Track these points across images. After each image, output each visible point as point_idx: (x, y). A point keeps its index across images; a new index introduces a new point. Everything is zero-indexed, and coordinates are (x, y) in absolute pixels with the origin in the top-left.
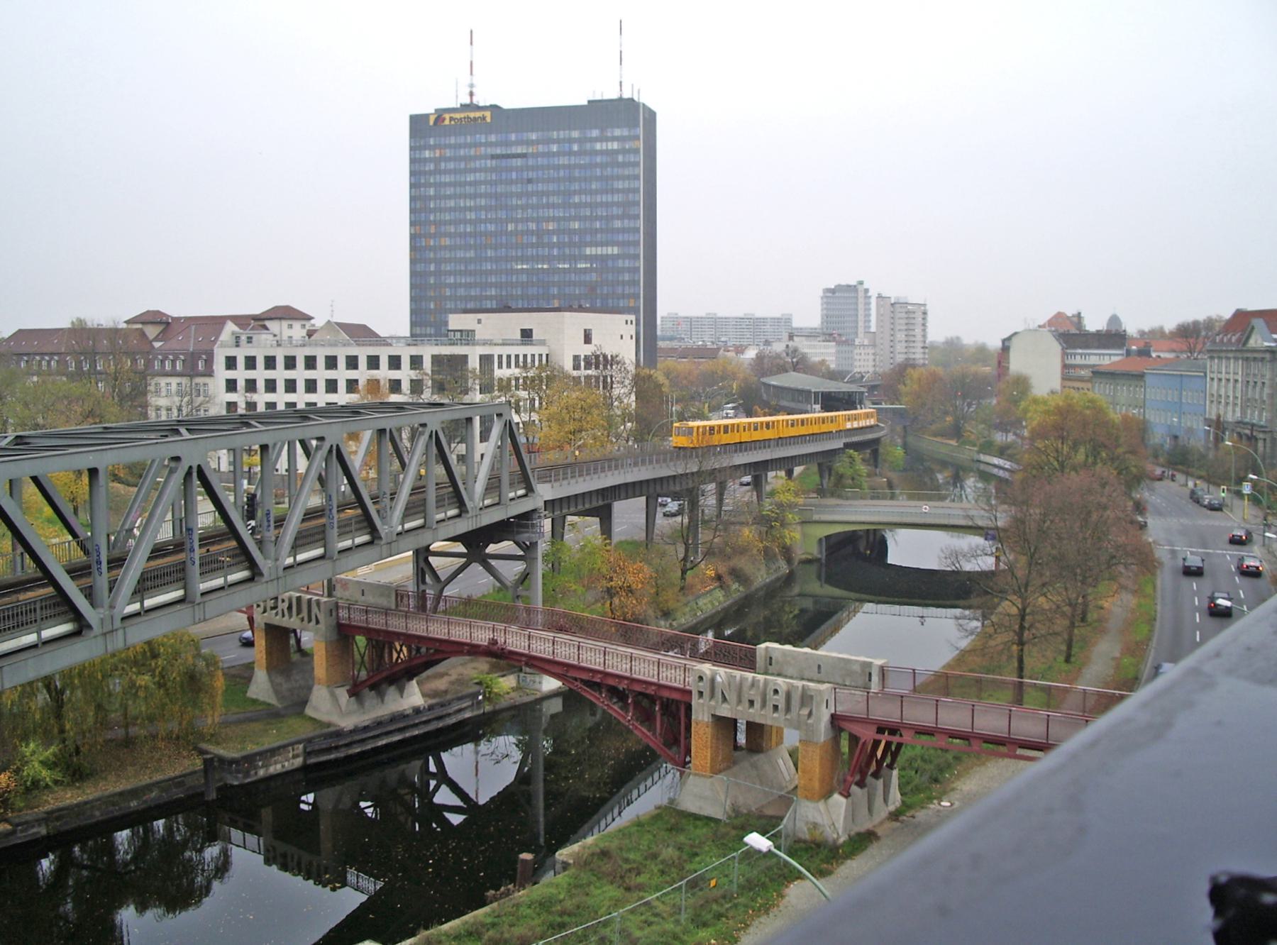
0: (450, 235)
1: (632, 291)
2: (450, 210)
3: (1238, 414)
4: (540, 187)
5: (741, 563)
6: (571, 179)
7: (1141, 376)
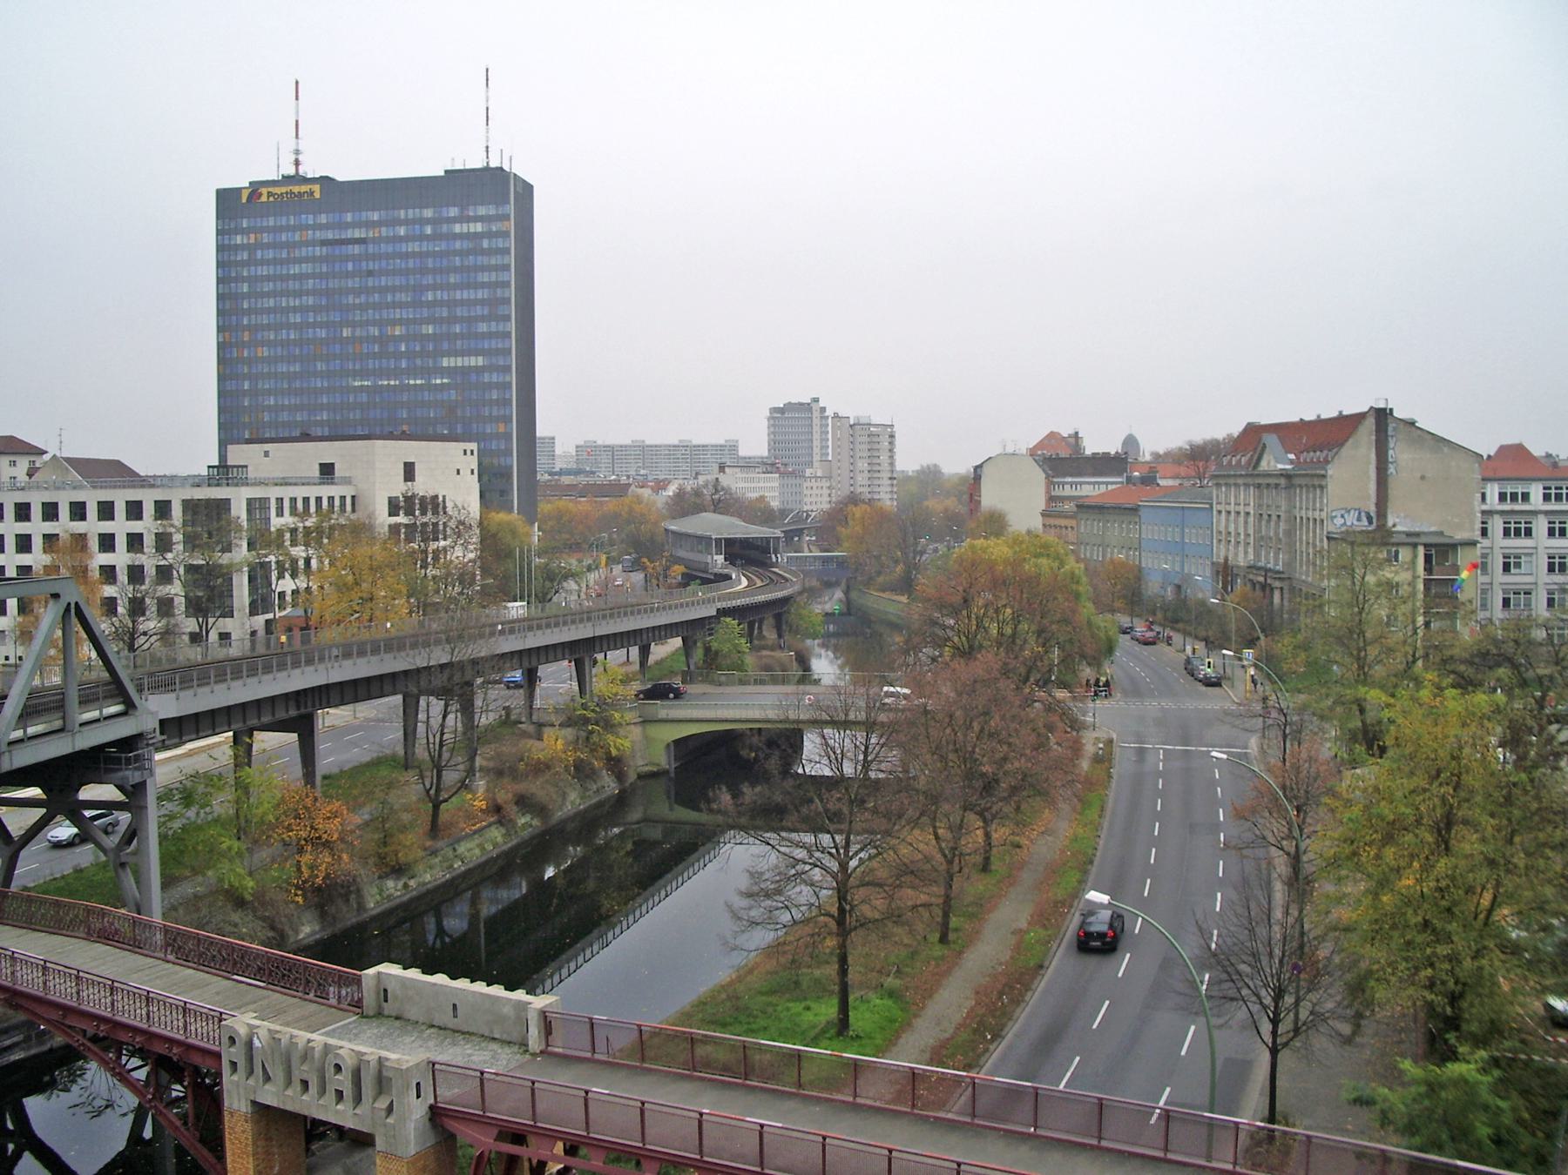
0: (270, 344)
1: (502, 412)
2: (269, 311)
3: (1251, 557)
4: (383, 281)
5: (536, 788)
6: (423, 271)
7: (1134, 510)
